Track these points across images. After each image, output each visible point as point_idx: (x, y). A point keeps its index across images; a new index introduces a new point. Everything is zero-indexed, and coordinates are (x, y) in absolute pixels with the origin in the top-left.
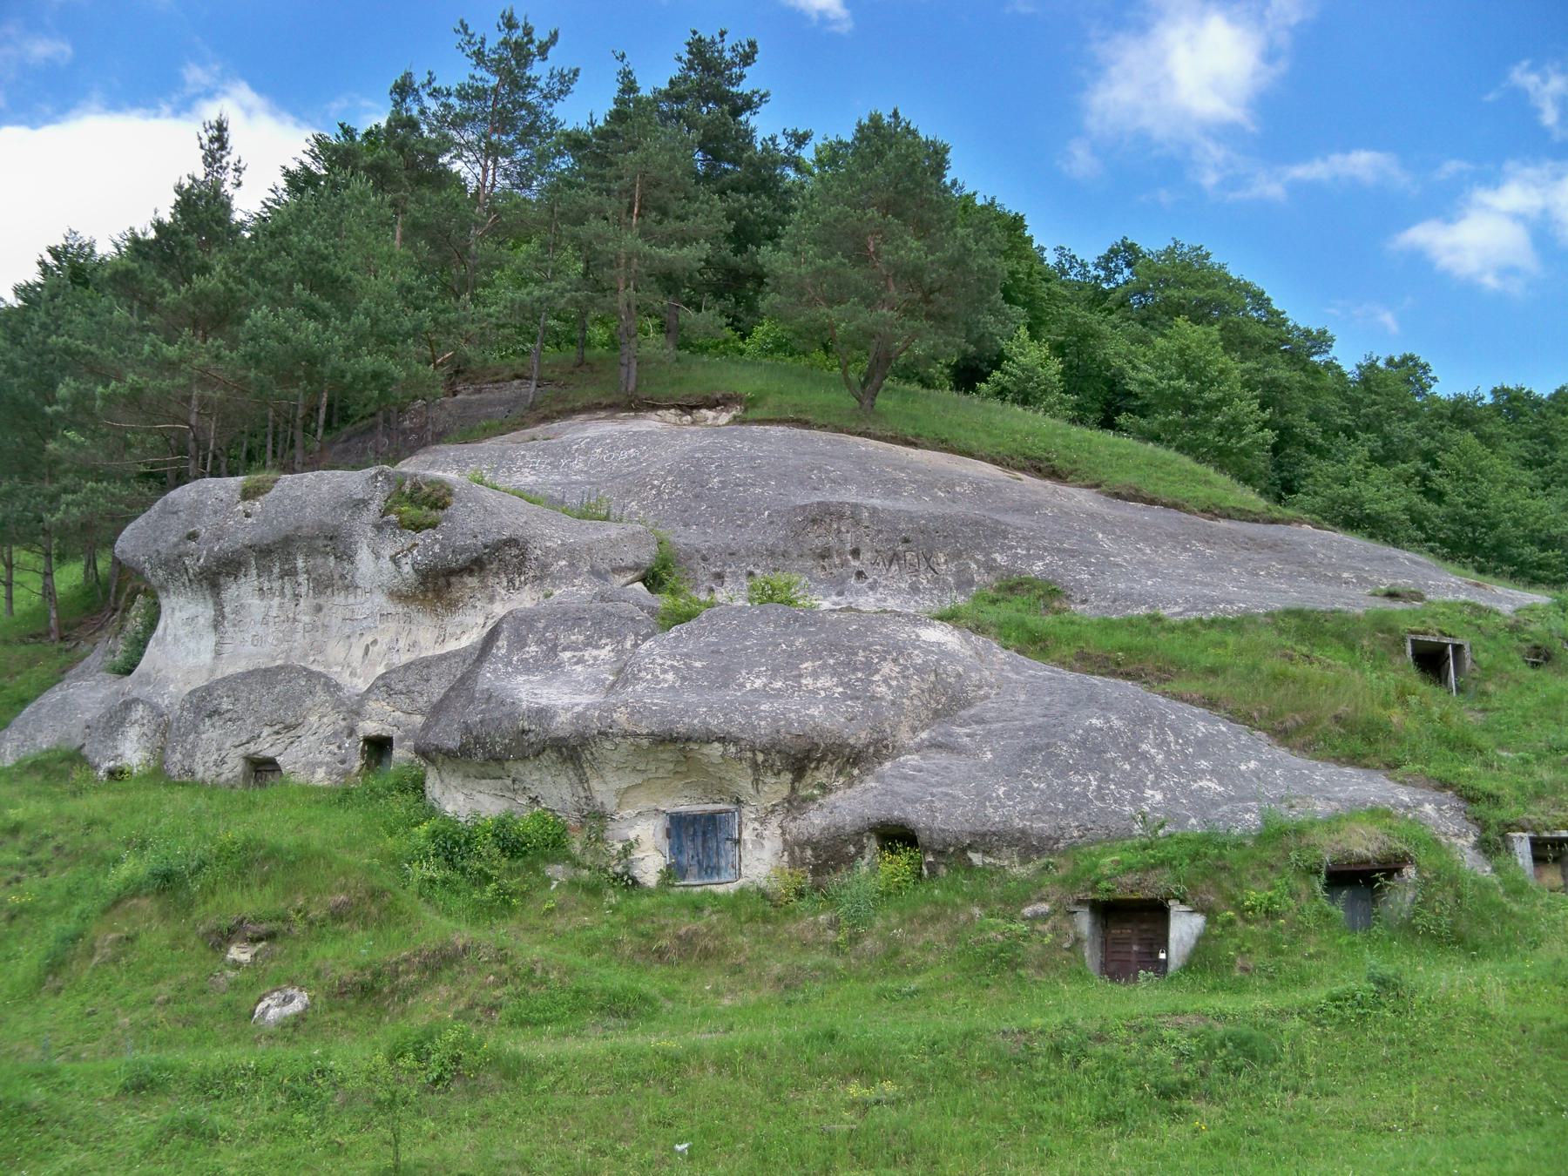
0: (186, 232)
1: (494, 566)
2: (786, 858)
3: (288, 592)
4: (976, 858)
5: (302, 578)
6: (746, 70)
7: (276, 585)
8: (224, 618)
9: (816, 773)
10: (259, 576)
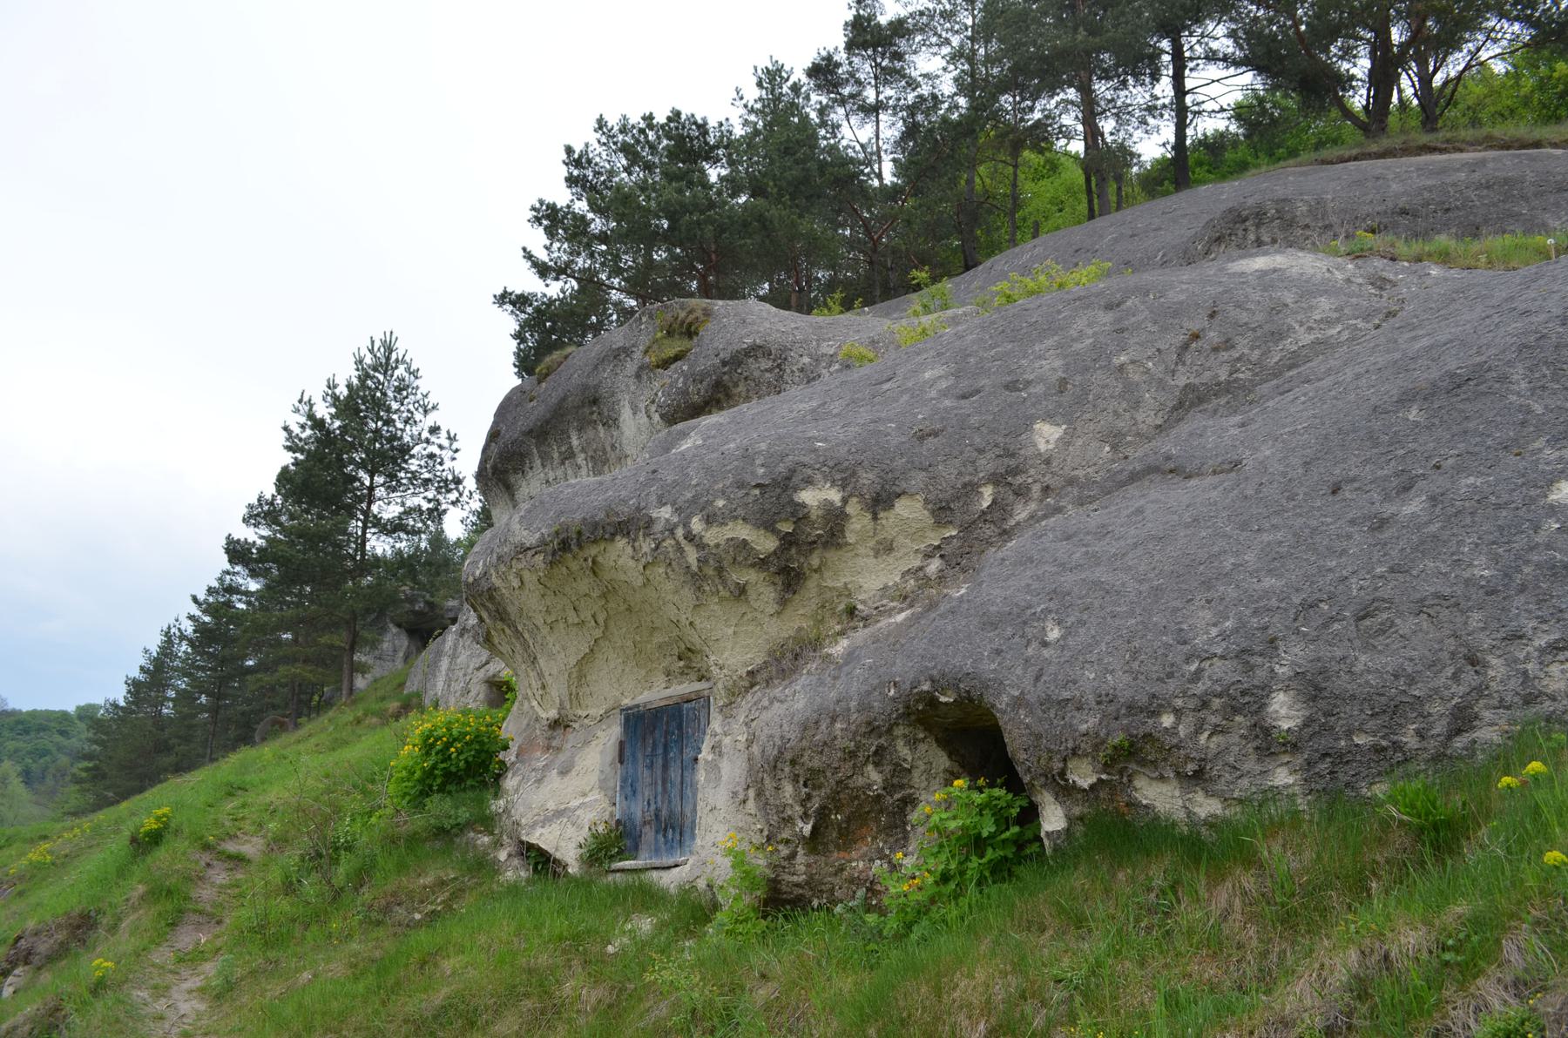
1: (741, 388)
2: (751, 805)
5: (580, 459)
7: (559, 473)
10: (543, 466)
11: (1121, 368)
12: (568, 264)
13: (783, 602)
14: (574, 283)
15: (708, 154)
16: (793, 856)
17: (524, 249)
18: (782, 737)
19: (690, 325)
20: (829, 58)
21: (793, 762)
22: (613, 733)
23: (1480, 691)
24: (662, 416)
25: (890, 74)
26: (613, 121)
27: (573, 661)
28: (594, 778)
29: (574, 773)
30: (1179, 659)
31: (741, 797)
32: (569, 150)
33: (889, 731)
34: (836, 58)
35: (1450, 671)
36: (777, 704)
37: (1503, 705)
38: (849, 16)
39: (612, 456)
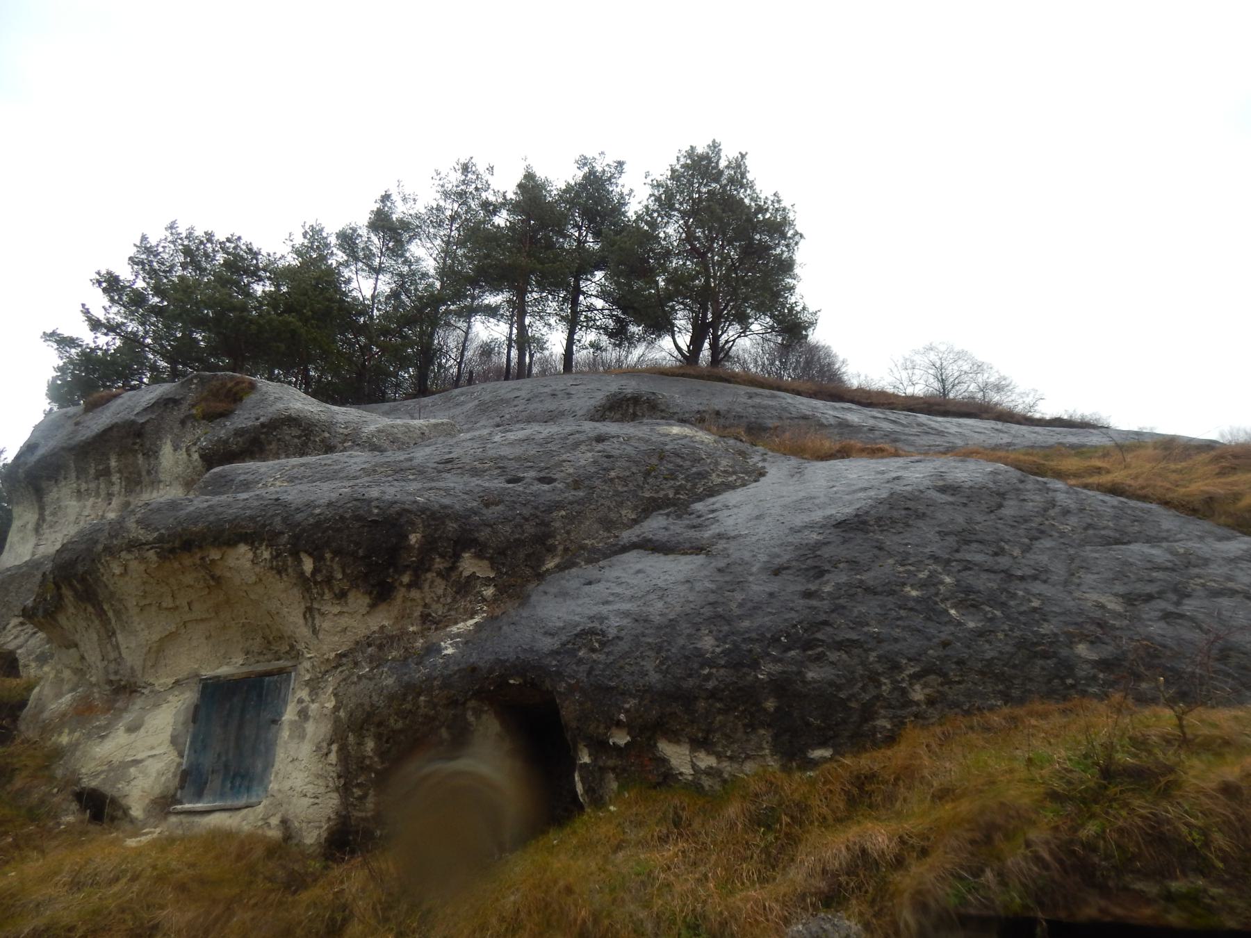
0: (249, 283)
1: (273, 446)
2: (333, 758)
3: (103, 493)
4: (679, 757)
5: (115, 478)
6: (995, 369)
7: (93, 485)
8: (44, 521)
9: (960, 718)
10: (78, 478)
11: (612, 480)
12: (119, 325)
13: (373, 606)
14: (118, 342)
15: (255, 274)
16: (364, 797)
17: (83, 305)
18: (372, 705)
19: (236, 394)
20: (354, 230)
21: (380, 724)
22: (186, 699)
23: (878, 697)
24: (201, 456)
25: (397, 250)
26: (182, 230)
27: (155, 637)
28: (166, 736)
29: (142, 730)
30: (696, 666)
31: (325, 751)
32: (144, 238)
33: (464, 703)
34: (359, 232)
35: (860, 685)
36: (365, 681)
37: (890, 706)
38: (375, 207)
39: (146, 479)
